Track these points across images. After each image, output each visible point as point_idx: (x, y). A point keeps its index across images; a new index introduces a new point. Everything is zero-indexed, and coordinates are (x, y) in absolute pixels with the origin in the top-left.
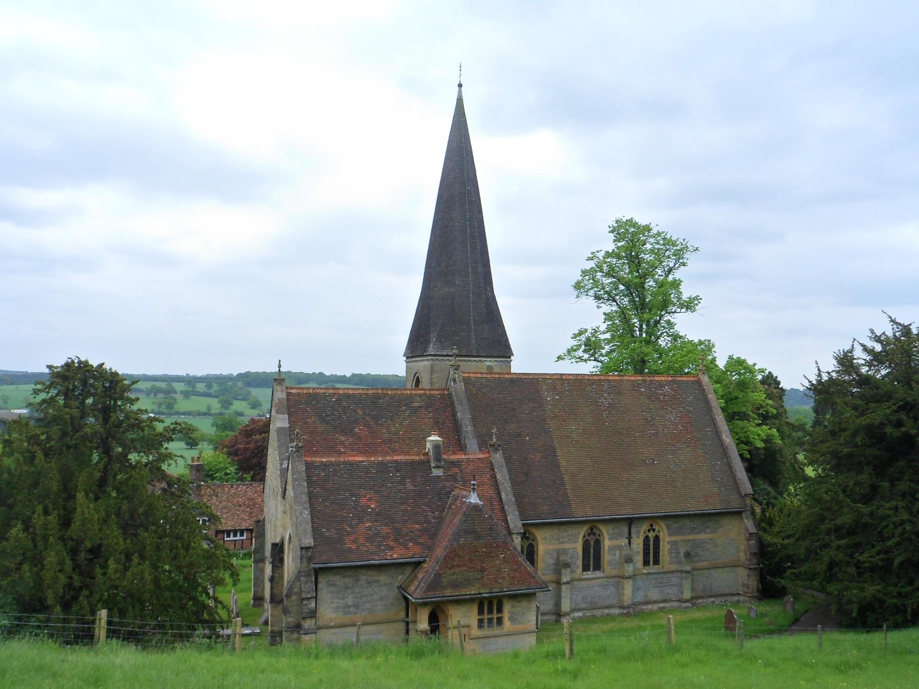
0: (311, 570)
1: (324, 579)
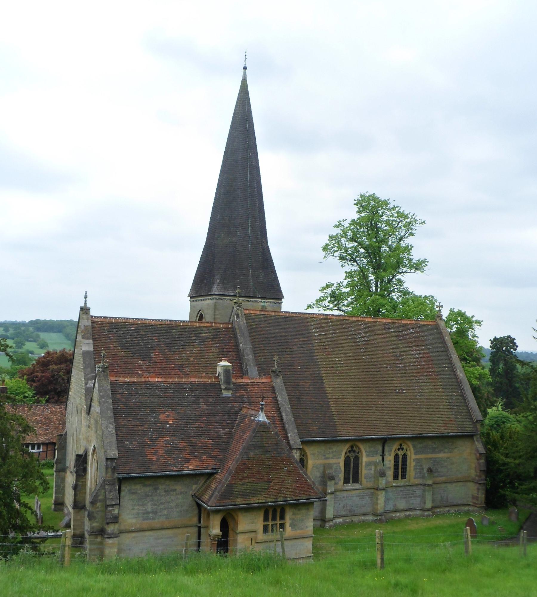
0: (114, 479)
1: (126, 487)
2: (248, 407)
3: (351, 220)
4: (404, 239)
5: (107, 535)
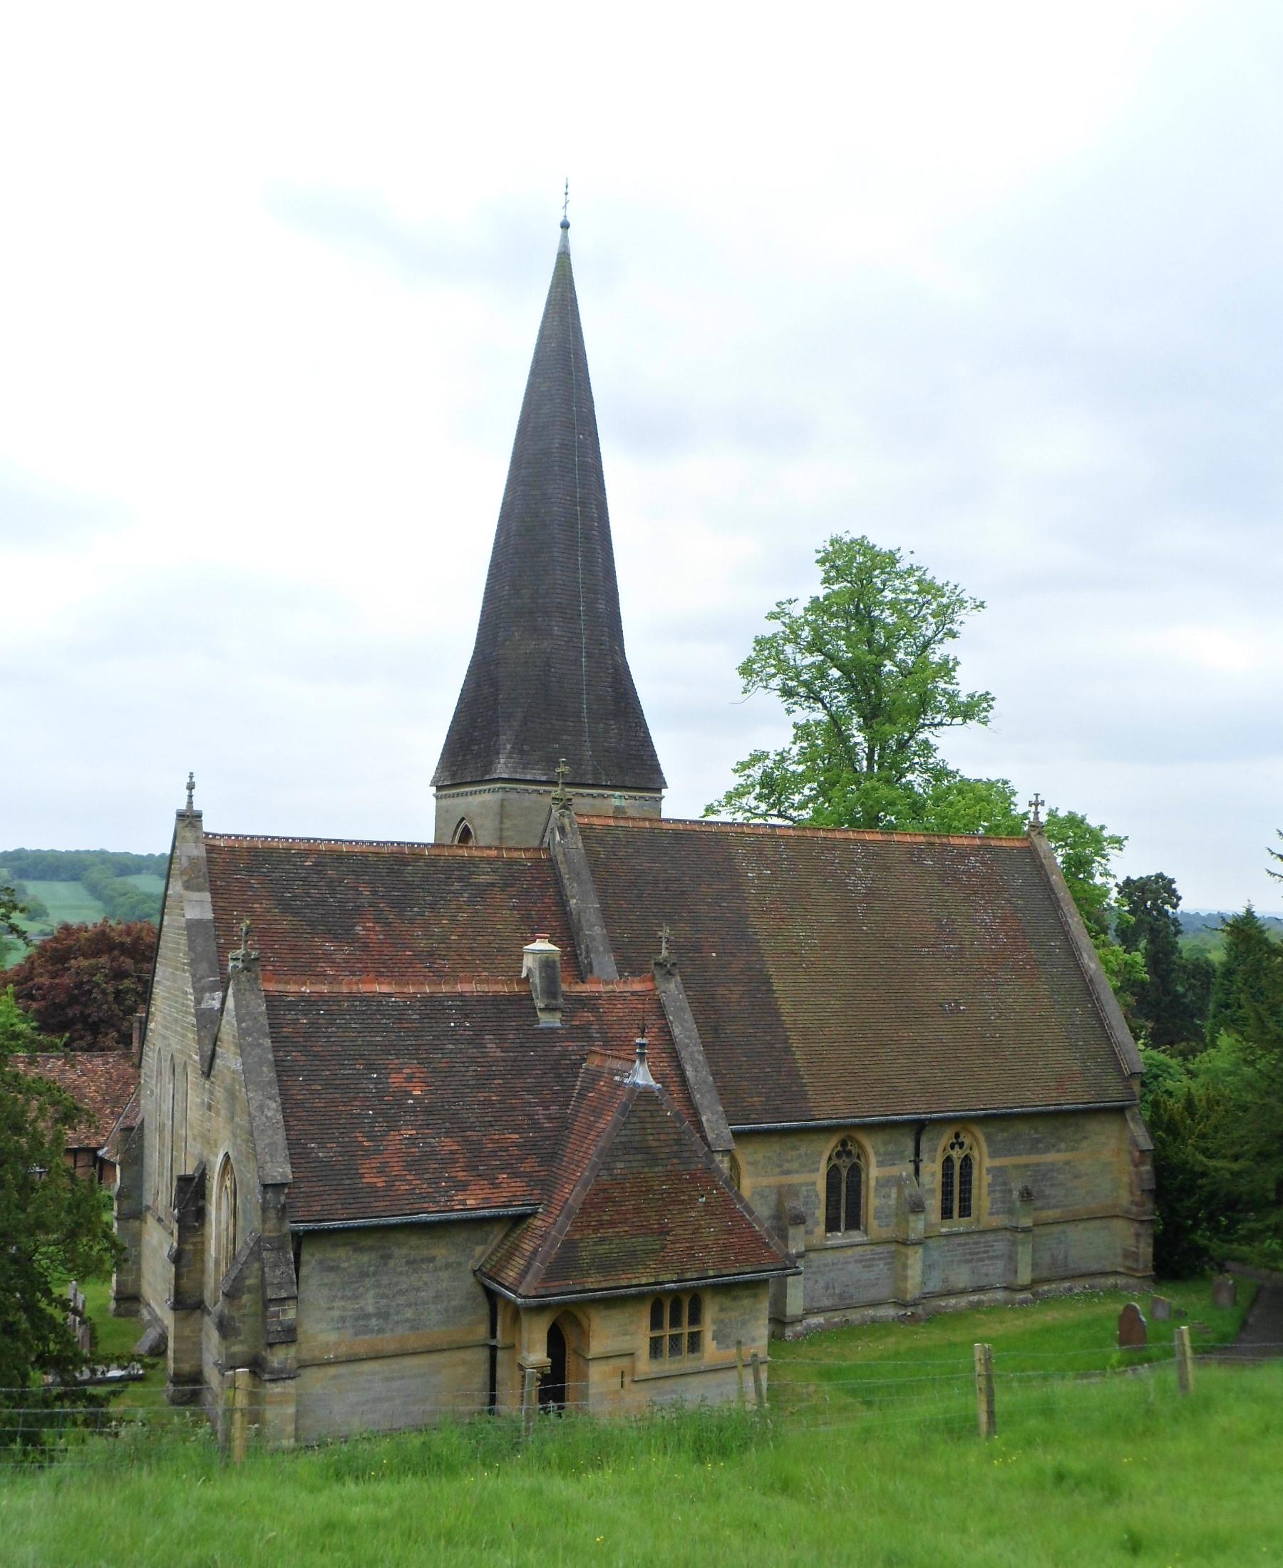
0: (285, 1236)
1: (312, 1255)
2: (603, 1052)
3: (810, 600)
4: (932, 646)
5: (270, 1373)
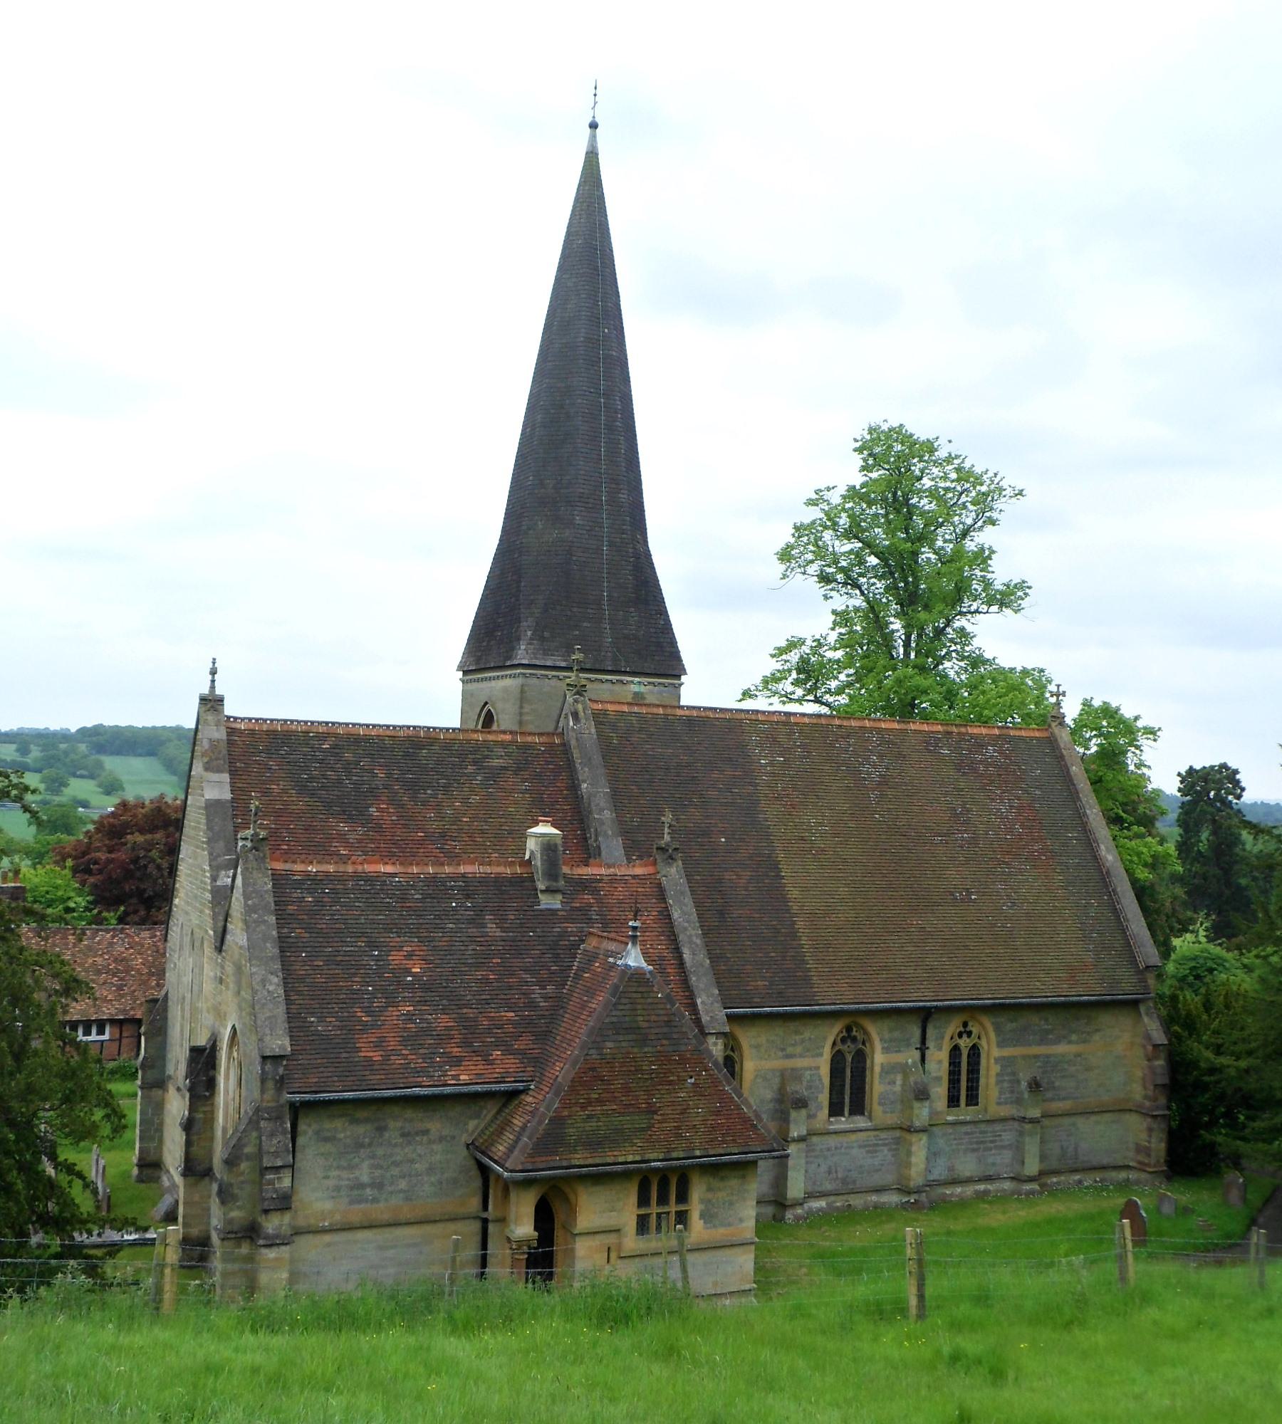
0: (282, 1106)
2: (600, 933)
4: (972, 534)
5: (264, 1238)
